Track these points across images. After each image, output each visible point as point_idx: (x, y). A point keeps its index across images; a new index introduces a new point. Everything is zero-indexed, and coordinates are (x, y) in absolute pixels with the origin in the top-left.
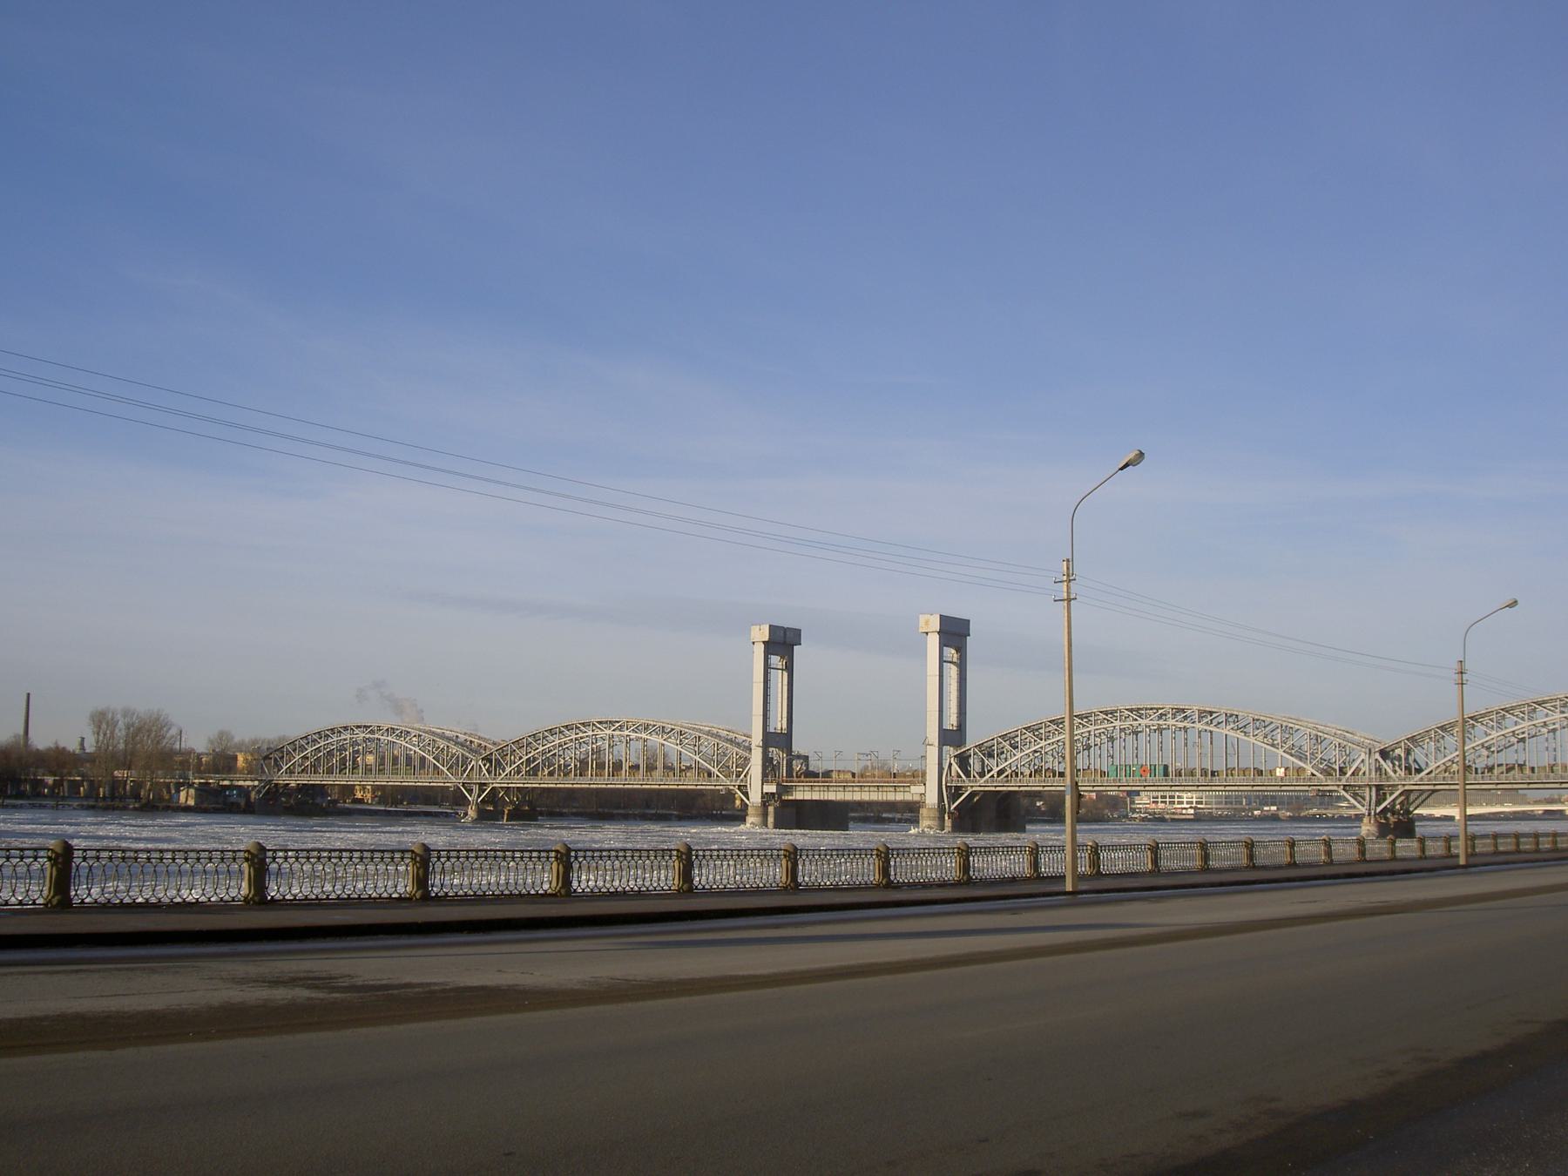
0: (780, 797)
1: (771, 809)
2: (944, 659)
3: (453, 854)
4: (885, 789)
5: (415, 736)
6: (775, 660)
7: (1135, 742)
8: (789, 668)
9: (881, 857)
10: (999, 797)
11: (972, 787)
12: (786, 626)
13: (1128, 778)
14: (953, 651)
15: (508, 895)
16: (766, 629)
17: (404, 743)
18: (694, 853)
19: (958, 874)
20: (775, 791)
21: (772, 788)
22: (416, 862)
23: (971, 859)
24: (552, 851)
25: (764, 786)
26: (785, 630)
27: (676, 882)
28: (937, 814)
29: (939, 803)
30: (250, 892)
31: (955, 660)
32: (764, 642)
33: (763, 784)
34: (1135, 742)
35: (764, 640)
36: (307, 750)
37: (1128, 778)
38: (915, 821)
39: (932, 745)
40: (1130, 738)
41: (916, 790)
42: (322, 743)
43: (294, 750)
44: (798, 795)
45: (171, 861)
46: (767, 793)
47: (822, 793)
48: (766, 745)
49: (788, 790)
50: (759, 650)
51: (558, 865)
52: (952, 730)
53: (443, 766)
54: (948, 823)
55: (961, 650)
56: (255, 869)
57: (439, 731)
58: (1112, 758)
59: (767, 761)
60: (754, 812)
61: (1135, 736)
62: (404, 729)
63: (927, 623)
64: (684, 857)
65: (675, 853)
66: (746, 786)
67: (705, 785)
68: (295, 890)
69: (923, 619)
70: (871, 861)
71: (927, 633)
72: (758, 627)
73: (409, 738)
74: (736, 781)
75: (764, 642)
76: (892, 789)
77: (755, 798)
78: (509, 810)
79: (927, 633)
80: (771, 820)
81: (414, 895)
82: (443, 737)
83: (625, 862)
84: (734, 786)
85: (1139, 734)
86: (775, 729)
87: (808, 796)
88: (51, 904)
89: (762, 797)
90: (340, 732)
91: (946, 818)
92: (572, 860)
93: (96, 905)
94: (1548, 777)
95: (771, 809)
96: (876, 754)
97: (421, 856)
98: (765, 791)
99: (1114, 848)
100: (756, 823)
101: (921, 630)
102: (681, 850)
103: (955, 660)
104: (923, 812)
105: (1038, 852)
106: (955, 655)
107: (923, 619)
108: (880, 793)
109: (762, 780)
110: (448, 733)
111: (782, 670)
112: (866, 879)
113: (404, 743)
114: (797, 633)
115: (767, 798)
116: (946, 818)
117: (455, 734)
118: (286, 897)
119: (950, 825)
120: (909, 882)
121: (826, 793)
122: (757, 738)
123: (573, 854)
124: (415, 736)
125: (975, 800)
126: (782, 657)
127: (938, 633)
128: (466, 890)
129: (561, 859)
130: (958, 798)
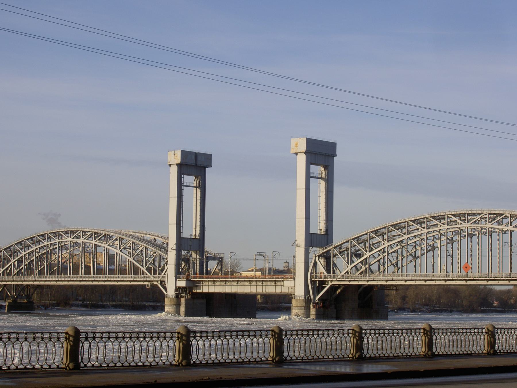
0: (191, 291)
1: (183, 300)
2: (312, 175)
3: (120, 335)
4: (268, 283)
5: (117, 240)
6: (189, 179)
7: (470, 243)
8: (202, 187)
9: (70, 341)
10: (361, 289)
11: (332, 281)
12: (197, 152)
13: (129, 275)
14: (322, 169)
15: (229, 363)
16: (179, 154)
17: (106, 246)
18: (363, 331)
19: (352, 352)
20: (184, 285)
21: (182, 283)
22: (356, 336)
23: (434, 338)
24: (175, 332)
25: (177, 282)
26: (196, 155)
27: (423, 349)
28: (303, 304)
29: (305, 296)
30: (67, 362)
31: (324, 176)
32: (177, 165)
33: (176, 280)
34: (470, 243)
35: (177, 163)
36: (21, 254)
37: (129, 275)
38: (288, 310)
39: (299, 246)
40: (464, 241)
41: (288, 283)
42: (34, 248)
43: (11, 255)
44: (205, 289)
45: (7, 340)
46: (179, 287)
47: (222, 287)
48: (179, 248)
49: (197, 284)
50: (174, 170)
51: (180, 343)
52: (198, 239)
53: (142, 266)
54: (313, 311)
55: (329, 167)
56: (183, 344)
57: (138, 234)
58: (452, 257)
59: (179, 259)
60: (169, 303)
61: (469, 239)
62: (106, 233)
63: (296, 145)
64: (276, 336)
65: (351, 332)
66: (165, 281)
67: (137, 281)
68: (231, 357)
69: (293, 141)
70: (171, 343)
71: (297, 154)
72: (173, 152)
73: (111, 241)
74: (159, 278)
75: (177, 165)
76: (273, 283)
77: (171, 292)
78: (9, 303)
79: (297, 154)
80: (183, 309)
81: (68, 366)
82: (142, 240)
83: (389, 337)
84: (157, 281)
85: (474, 237)
86: (191, 235)
87: (211, 290)
88: (356, 357)
89: (176, 291)
90: (50, 238)
91: (312, 307)
92: (283, 337)
93: (308, 360)
94: (399, 277)
95: (183, 300)
96: (275, 253)
97: (277, 333)
98: (178, 285)
99: (205, 334)
100: (170, 311)
101: (292, 151)
102: (181, 332)
103: (324, 176)
104: (294, 301)
105: (282, 335)
106: (324, 173)
107: (293, 141)
108: (264, 287)
109: (176, 277)
110: (146, 237)
111: (197, 187)
112: (407, 351)
113: (106, 246)
114: (208, 158)
115: (179, 291)
116: (312, 307)
117: (153, 237)
118: (138, 364)
119: (314, 313)
120: (504, 352)
121: (224, 287)
122: (172, 242)
123: (192, 335)
124: (117, 240)
125: (338, 292)
126: (197, 177)
127: (305, 153)
128: (34, 364)
129: (182, 338)
130: (322, 290)
